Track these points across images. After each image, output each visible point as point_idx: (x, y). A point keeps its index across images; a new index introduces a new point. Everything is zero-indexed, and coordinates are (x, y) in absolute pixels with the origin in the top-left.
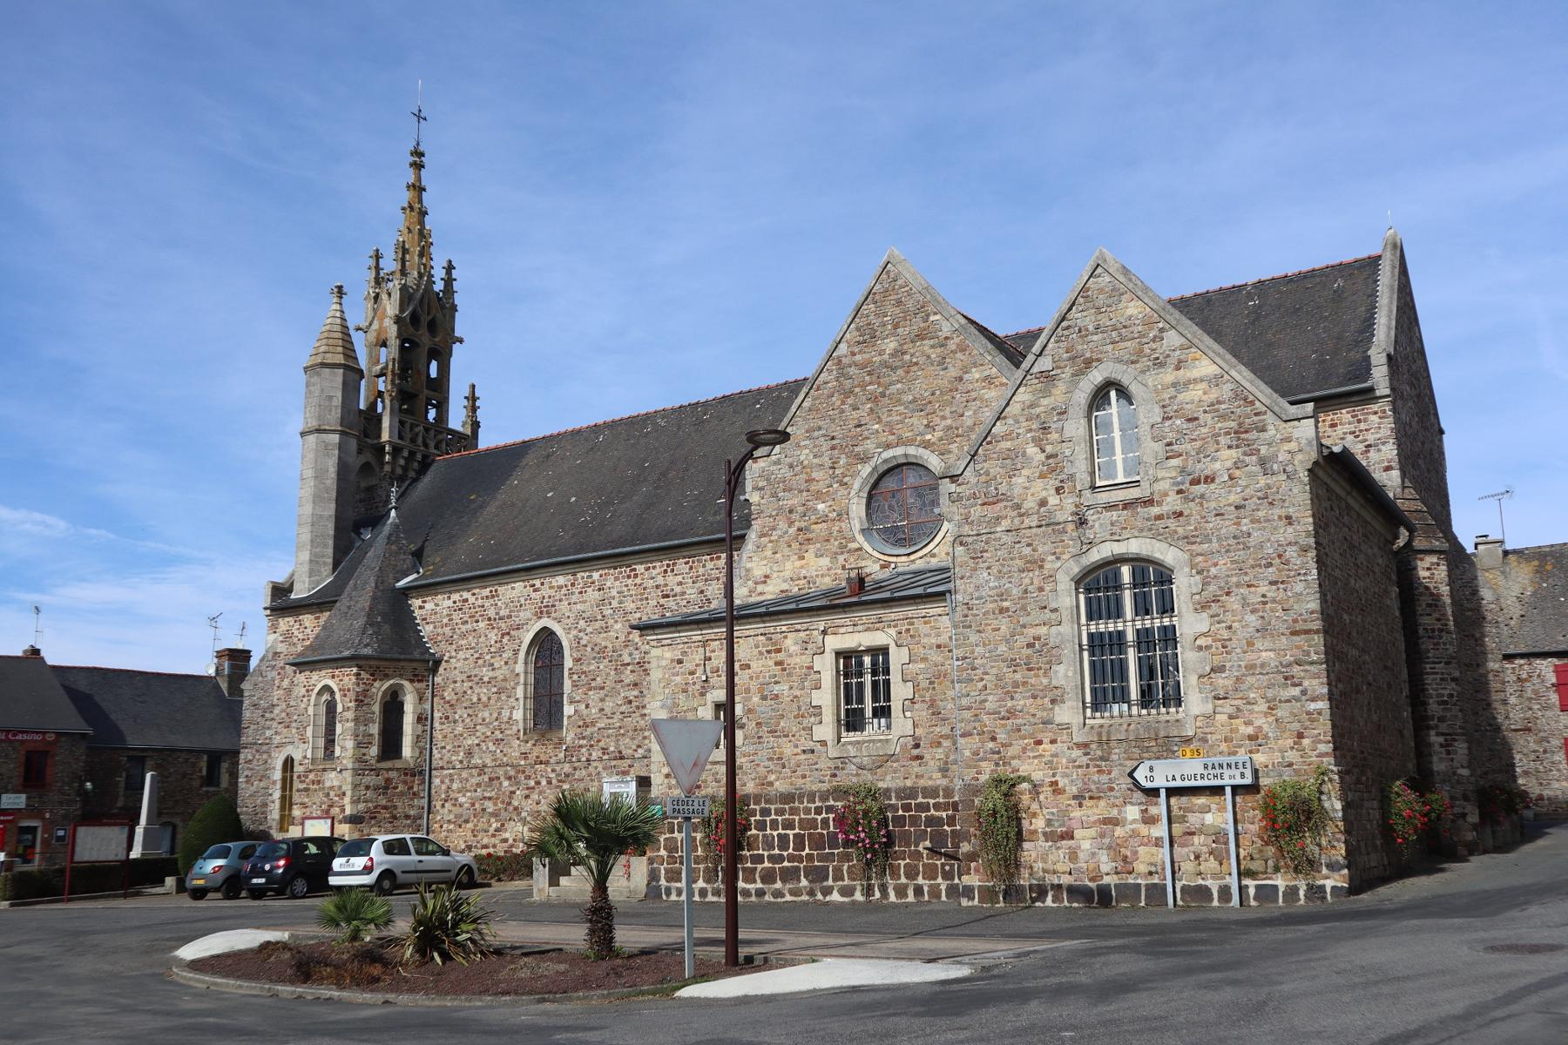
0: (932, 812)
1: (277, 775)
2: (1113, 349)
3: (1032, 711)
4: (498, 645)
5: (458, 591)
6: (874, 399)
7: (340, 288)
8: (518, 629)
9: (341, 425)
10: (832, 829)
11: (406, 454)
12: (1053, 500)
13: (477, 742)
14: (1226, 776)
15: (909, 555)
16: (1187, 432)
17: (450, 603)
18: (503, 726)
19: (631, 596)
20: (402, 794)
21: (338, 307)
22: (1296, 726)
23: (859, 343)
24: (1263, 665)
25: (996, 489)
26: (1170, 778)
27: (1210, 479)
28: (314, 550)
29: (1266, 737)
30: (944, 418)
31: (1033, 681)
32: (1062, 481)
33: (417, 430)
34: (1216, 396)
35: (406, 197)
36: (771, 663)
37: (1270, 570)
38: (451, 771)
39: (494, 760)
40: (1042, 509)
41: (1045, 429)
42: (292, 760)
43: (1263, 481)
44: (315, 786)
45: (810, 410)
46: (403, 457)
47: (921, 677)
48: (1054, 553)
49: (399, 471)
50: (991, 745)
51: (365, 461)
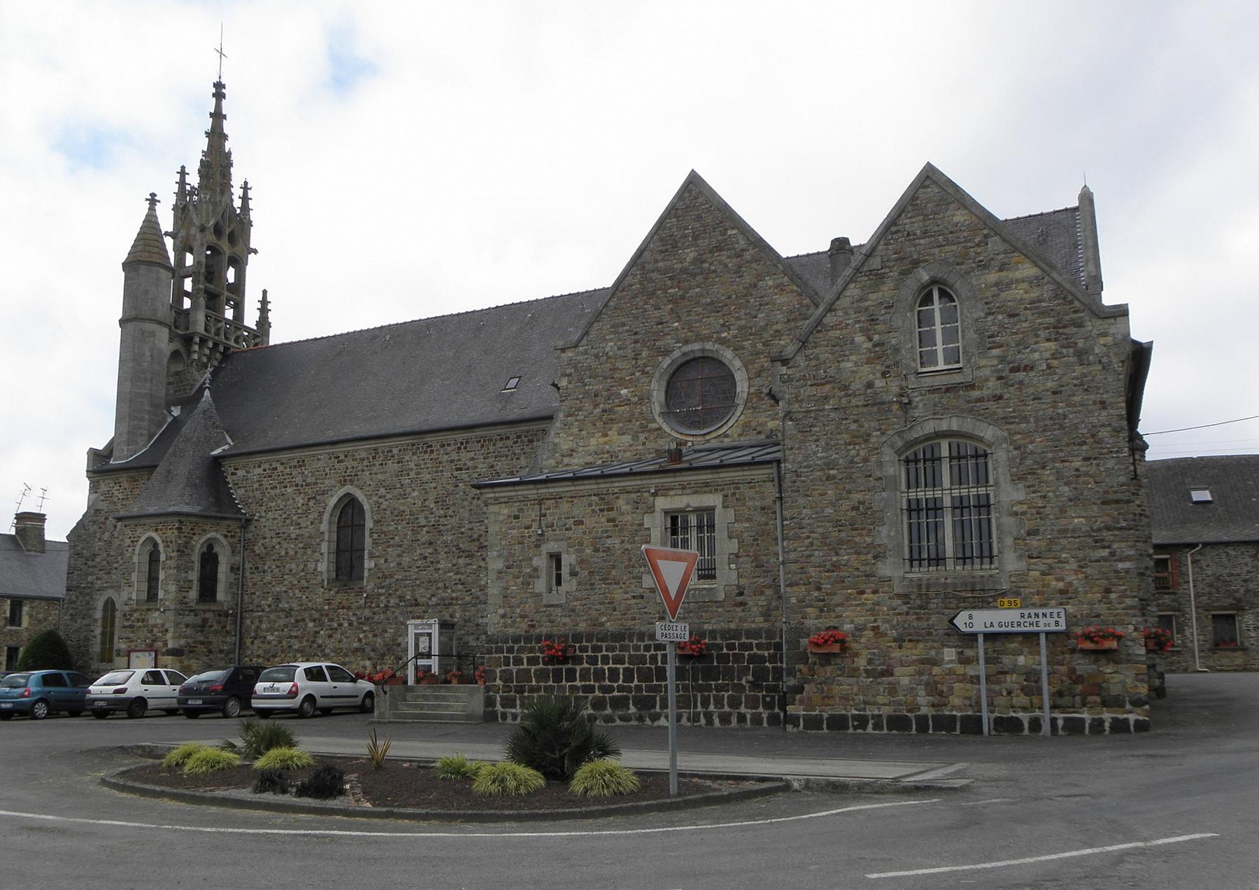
0: (755, 650)
1: (98, 614)
2: (940, 252)
3: (856, 565)
4: (305, 507)
6: (674, 300)
10: (659, 664)
11: (210, 344)
12: (879, 383)
13: (284, 589)
14: (1041, 624)
15: (705, 435)
16: (1009, 326)
18: (309, 577)
19: (428, 468)
20: (216, 632)
22: (1104, 582)
23: (662, 252)
24: (1074, 530)
25: (825, 372)
26: (988, 625)
27: (1029, 368)
29: (1076, 591)
30: (738, 319)
31: (857, 539)
32: (888, 367)
34: (1037, 295)
35: (208, 124)
36: (604, 520)
37: (1084, 447)
38: (261, 614)
39: (301, 605)
40: (869, 391)
41: (873, 320)
42: (113, 603)
43: (1079, 370)
44: (140, 624)
45: (615, 309)
47: (745, 535)
48: (880, 429)
50: (816, 594)
51: (175, 349)
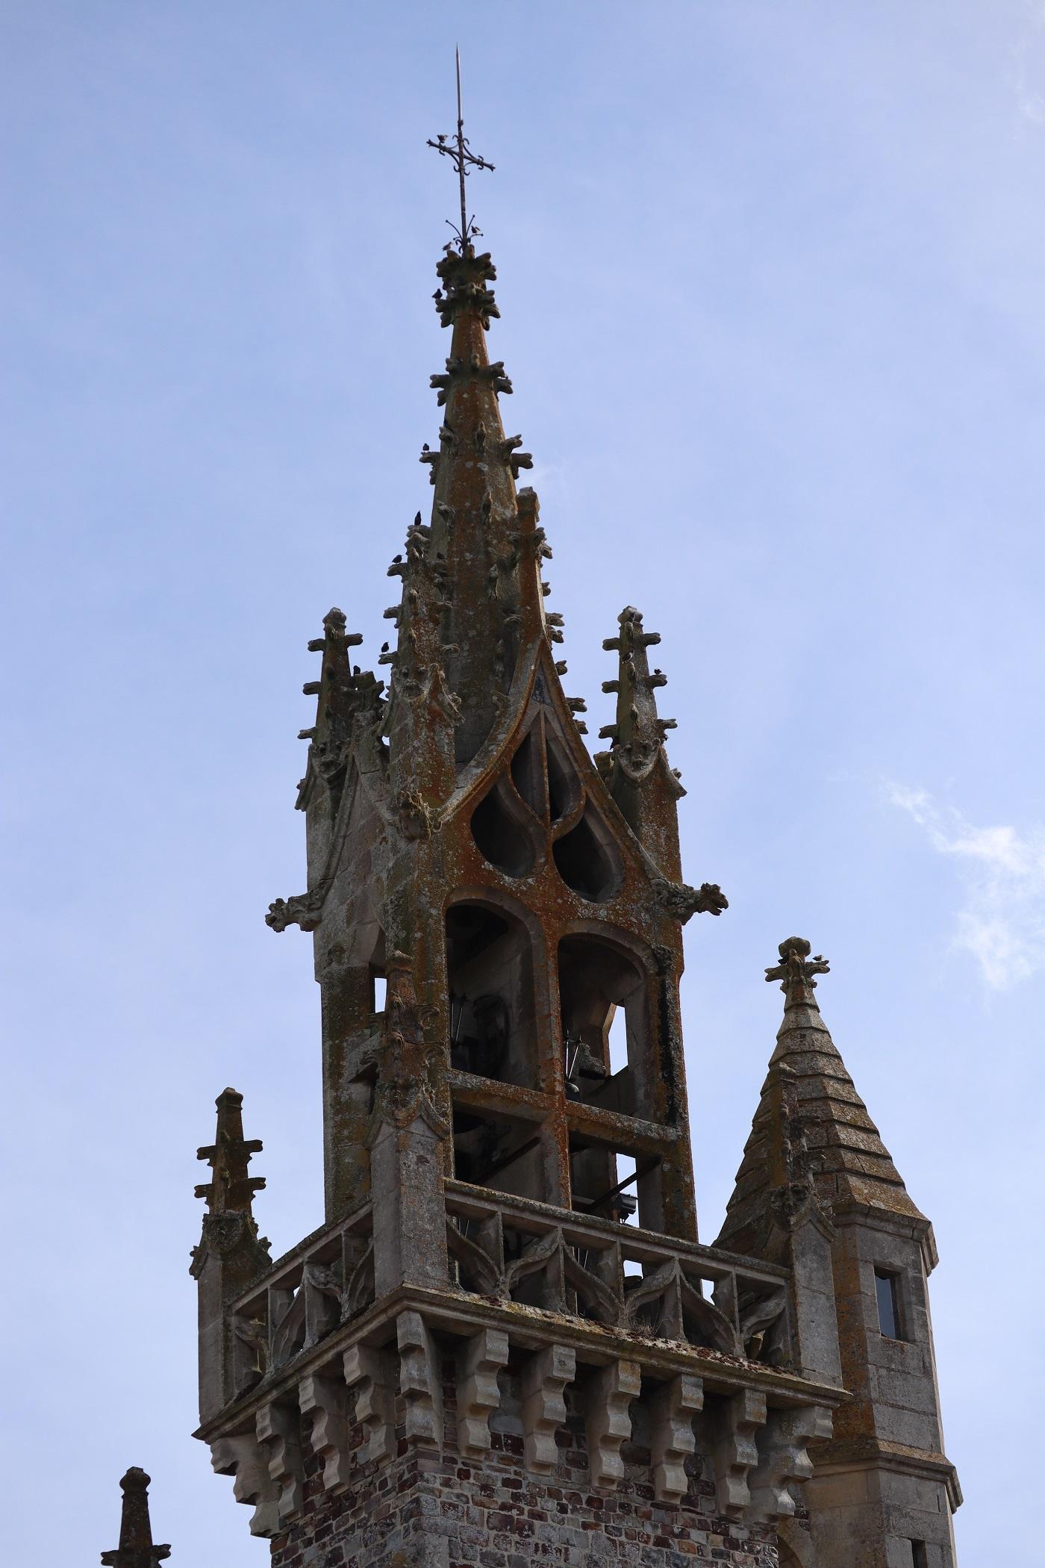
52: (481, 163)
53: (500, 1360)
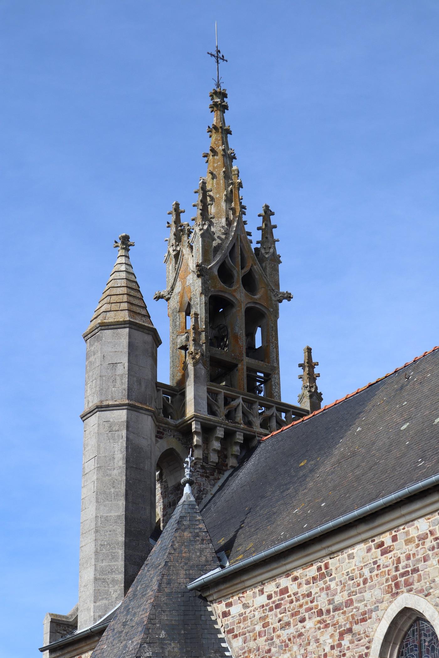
5: (273, 578)
7: (125, 240)
8: (364, 620)
9: (128, 399)
11: (220, 433)
17: (262, 600)
21: (123, 260)
28: (100, 564)
33: (234, 403)
46: (217, 439)
49: (214, 458)
51: (166, 447)
52: (212, 55)
53: (221, 436)
